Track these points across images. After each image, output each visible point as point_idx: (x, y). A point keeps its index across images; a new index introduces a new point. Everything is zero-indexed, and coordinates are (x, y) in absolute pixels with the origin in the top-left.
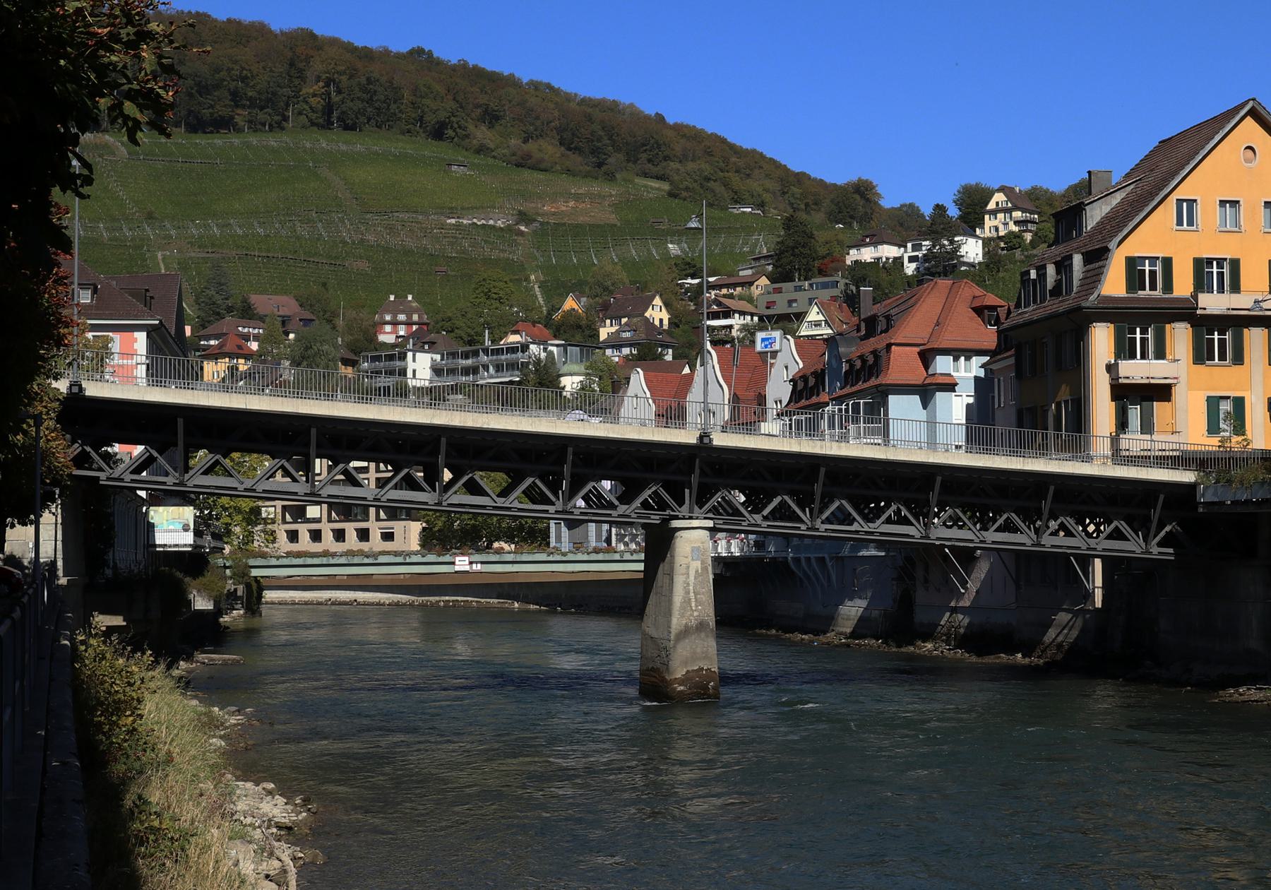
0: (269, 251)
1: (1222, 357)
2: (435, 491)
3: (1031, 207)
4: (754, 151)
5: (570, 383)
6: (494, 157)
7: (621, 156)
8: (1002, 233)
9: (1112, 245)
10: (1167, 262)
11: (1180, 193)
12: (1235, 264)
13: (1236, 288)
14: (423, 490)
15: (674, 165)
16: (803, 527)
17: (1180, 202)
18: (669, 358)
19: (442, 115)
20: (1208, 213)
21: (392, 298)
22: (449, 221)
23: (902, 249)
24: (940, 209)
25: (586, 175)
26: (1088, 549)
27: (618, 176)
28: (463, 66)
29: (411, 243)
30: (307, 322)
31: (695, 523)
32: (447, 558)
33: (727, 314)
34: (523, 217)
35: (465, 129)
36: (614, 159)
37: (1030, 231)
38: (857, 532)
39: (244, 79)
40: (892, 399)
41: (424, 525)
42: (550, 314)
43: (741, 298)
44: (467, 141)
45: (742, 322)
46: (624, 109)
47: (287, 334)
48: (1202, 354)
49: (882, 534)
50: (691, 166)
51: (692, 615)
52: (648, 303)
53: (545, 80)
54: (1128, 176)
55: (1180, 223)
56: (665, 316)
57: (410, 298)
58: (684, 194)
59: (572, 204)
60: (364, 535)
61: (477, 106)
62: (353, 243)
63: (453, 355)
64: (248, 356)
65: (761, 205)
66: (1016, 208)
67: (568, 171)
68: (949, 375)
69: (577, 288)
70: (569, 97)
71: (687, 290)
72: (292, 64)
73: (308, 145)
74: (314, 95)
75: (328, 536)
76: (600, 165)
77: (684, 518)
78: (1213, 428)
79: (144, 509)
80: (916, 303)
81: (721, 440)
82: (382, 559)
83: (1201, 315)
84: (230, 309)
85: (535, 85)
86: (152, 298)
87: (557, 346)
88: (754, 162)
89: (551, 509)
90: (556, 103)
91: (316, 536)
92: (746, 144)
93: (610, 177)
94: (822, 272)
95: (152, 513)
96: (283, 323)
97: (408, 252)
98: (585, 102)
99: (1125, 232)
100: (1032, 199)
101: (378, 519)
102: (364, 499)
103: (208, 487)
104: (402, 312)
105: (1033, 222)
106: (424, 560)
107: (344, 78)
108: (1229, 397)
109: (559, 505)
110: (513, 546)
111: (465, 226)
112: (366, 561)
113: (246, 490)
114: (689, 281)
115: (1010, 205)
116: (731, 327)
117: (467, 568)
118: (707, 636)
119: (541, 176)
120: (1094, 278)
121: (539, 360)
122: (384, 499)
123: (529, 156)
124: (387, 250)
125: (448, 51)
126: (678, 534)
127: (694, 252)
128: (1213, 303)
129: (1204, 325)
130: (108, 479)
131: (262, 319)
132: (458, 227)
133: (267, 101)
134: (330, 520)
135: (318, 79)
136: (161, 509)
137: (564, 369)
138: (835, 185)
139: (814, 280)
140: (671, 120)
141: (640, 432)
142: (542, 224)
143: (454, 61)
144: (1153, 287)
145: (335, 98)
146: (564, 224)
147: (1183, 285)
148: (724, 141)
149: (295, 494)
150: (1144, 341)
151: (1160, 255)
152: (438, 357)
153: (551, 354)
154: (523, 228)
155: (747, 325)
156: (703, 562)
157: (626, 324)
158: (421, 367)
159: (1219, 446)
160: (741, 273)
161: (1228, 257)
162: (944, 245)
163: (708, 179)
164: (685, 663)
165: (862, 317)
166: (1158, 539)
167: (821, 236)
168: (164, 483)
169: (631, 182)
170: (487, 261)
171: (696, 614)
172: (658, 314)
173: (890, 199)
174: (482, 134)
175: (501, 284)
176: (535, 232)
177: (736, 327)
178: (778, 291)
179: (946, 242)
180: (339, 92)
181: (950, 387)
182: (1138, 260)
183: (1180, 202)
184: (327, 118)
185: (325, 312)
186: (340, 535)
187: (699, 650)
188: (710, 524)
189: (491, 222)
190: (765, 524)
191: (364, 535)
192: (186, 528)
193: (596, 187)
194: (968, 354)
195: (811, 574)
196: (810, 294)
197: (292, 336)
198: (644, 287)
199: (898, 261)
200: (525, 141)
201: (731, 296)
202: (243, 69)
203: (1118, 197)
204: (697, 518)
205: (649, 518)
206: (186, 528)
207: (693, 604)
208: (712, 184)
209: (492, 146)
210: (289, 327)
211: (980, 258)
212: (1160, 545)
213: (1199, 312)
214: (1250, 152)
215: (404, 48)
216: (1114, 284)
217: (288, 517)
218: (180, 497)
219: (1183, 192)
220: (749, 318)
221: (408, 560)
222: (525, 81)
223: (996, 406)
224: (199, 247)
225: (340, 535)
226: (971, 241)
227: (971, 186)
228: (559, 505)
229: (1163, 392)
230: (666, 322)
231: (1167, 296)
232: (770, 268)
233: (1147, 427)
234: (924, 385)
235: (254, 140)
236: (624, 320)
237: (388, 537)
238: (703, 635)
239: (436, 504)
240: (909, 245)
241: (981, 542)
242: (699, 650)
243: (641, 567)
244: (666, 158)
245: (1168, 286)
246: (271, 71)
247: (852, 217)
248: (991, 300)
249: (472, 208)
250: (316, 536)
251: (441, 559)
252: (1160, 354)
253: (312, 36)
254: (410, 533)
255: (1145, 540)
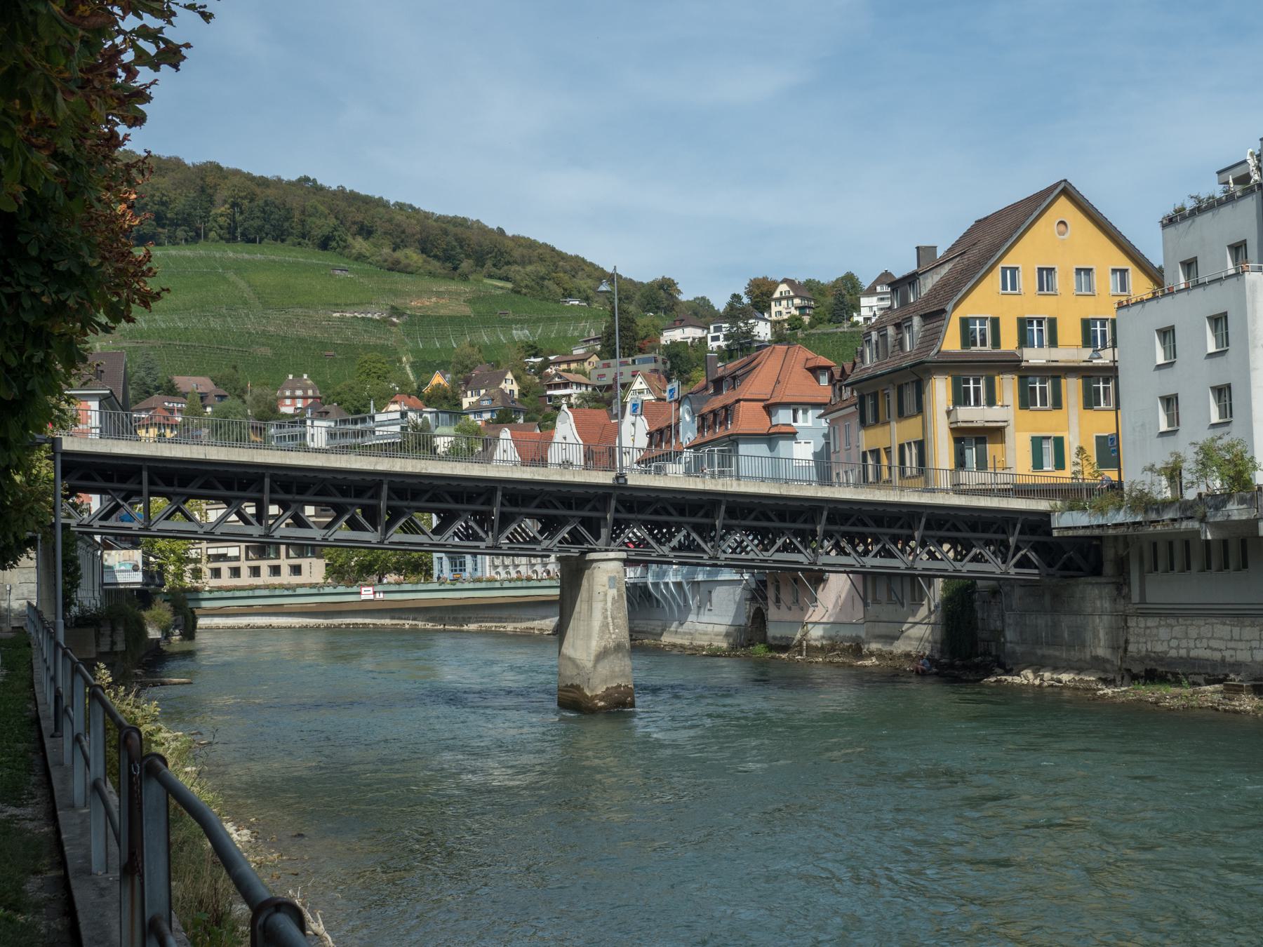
0: (188, 341)
1: (1044, 402)
2: (377, 530)
3: (808, 295)
4: (577, 257)
5: (442, 443)
6: (371, 264)
7: (471, 261)
8: (786, 317)
9: (949, 308)
10: (995, 322)
11: (1006, 262)
12: (1053, 323)
13: (1053, 342)
14: (365, 530)
15: (516, 268)
16: (706, 557)
17: (1004, 269)
18: (521, 421)
19: (326, 231)
20: (1028, 281)
21: (291, 377)
22: (335, 315)
23: (706, 331)
24: (736, 297)
25: (445, 277)
26: (955, 571)
27: (470, 277)
28: (342, 190)
29: (303, 333)
30: (222, 397)
31: (612, 555)
32: (355, 589)
33: (566, 385)
34: (395, 311)
35: (345, 241)
36: (466, 265)
37: (808, 315)
38: (753, 560)
39: (163, 203)
40: (743, 449)
41: (327, 561)
42: (420, 388)
43: (577, 372)
44: (347, 250)
45: (579, 391)
46: (472, 225)
47: (205, 407)
48: (1026, 400)
49: (775, 561)
50: (529, 268)
51: (610, 638)
52: (502, 378)
53: (408, 202)
54: (950, 250)
55: (1005, 288)
56: (515, 388)
57: (305, 376)
58: (524, 291)
59: (434, 300)
60: (276, 570)
61: (354, 223)
62: (257, 333)
63: (344, 422)
64: (172, 427)
65: (587, 299)
66: (796, 296)
67: (430, 274)
68: (790, 425)
69: (443, 367)
70: (427, 216)
71: (532, 367)
72: (203, 190)
73: (218, 255)
74: (222, 215)
75: (245, 572)
76: (455, 269)
77: (600, 551)
78: (1038, 464)
79: (99, 552)
80: (758, 365)
81: (635, 480)
82: (299, 591)
83: (1026, 367)
84: (157, 388)
85: (401, 206)
86: (102, 371)
87: (430, 413)
88: (578, 265)
89: (482, 545)
90: (418, 220)
91: (236, 572)
92: (570, 251)
93: (465, 278)
94: (641, 351)
95: (105, 556)
96: (202, 398)
97: (302, 340)
98: (440, 219)
99: (960, 295)
100: (808, 290)
101: (288, 557)
102: (314, 539)
103: (171, 531)
104: (300, 388)
105: (810, 307)
106: (335, 591)
107: (246, 202)
108: (1049, 438)
109: (489, 541)
110: (402, 577)
111: (348, 318)
112: (286, 593)
113: (205, 533)
114: (532, 360)
115: (792, 294)
116: (569, 396)
117: (372, 597)
118: (624, 656)
119: (408, 278)
120: (934, 337)
121: (417, 424)
122: (331, 539)
123: (398, 262)
124: (284, 339)
125: (330, 180)
126: (595, 565)
127: (534, 336)
128: (1035, 356)
129: (1026, 374)
130: (79, 525)
131: (184, 395)
132: (342, 319)
133: (185, 220)
134: (247, 559)
135: (225, 202)
136: (113, 552)
137: (438, 431)
138: (642, 283)
139: (636, 357)
140: (509, 233)
141: (562, 475)
142: (410, 316)
143: (334, 187)
144: (983, 343)
145: (239, 218)
146: (429, 316)
147: (1009, 341)
148: (553, 249)
149: (251, 536)
150: (977, 390)
151: (989, 315)
152: (333, 424)
153: (426, 419)
154: (395, 320)
155: (583, 394)
156: (618, 590)
157: (485, 395)
158: (318, 432)
159: (1072, 478)
160: (575, 352)
161: (1047, 316)
162: (740, 327)
163: (543, 278)
164: (605, 681)
165: (710, 379)
166: (1015, 560)
167: (641, 321)
168: (130, 529)
169: (482, 281)
170: (367, 348)
171: (613, 636)
172: (510, 385)
173: (686, 295)
174: (359, 244)
175: (379, 365)
176: (405, 324)
177: (574, 396)
178: (608, 366)
179: (742, 325)
180: (241, 213)
181: (792, 435)
182: (971, 321)
183: (1004, 269)
184: (231, 235)
185: (235, 389)
186: (256, 571)
187: (617, 669)
188: (623, 555)
189: (369, 315)
190: (672, 554)
191: (276, 570)
192: (135, 569)
193: (453, 286)
194: (805, 407)
195: (669, 596)
196: (634, 368)
197: (209, 409)
198: (497, 365)
199: (703, 341)
200: (394, 250)
201: (569, 371)
202: (163, 195)
203: (947, 268)
204: (612, 551)
205: (569, 551)
206: (135, 569)
207: (611, 628)
208: (546, 283)
209: (368, 254)
210: (206, 402)
211: (769, 337)
212: (1016, 566)
213: (1023, 364)
214: (1062, 227)
215: (294, 177)
216: (951, 342)
217: (291, 553)
218: (132, 541)
219: (1007, 262)
220: (584, 389)
221: (322, 591)
222: (392, 202)
223: (832, 450)
224: (130, 338)
225: (256, 571)
226: (762, 323)
227: (759, 280)
228: (489, 541)
229: (995, 433)
230: (516, 393)
231: (996, 351)
232: (599, 348)
233: (982, 465)
234: (769, 434)
235: (173, 251)
236: (483, 392)
237: (296, 570)
238: (620, 655)
239: (378, 543)
240: (712, 327)
241: (862, 566)
242: (617, 669)
243: (557, 591)
244: (508, 263)
245: (996, 342)
246: (186, 196)
247: (658, 308)
248: (823, 361)
249: (354, 304)
250: (236, 572)
251: (349, 590)
252: (991, 402)
253: (218, 168)
254: (314, 569)
255: (1004, 562)
